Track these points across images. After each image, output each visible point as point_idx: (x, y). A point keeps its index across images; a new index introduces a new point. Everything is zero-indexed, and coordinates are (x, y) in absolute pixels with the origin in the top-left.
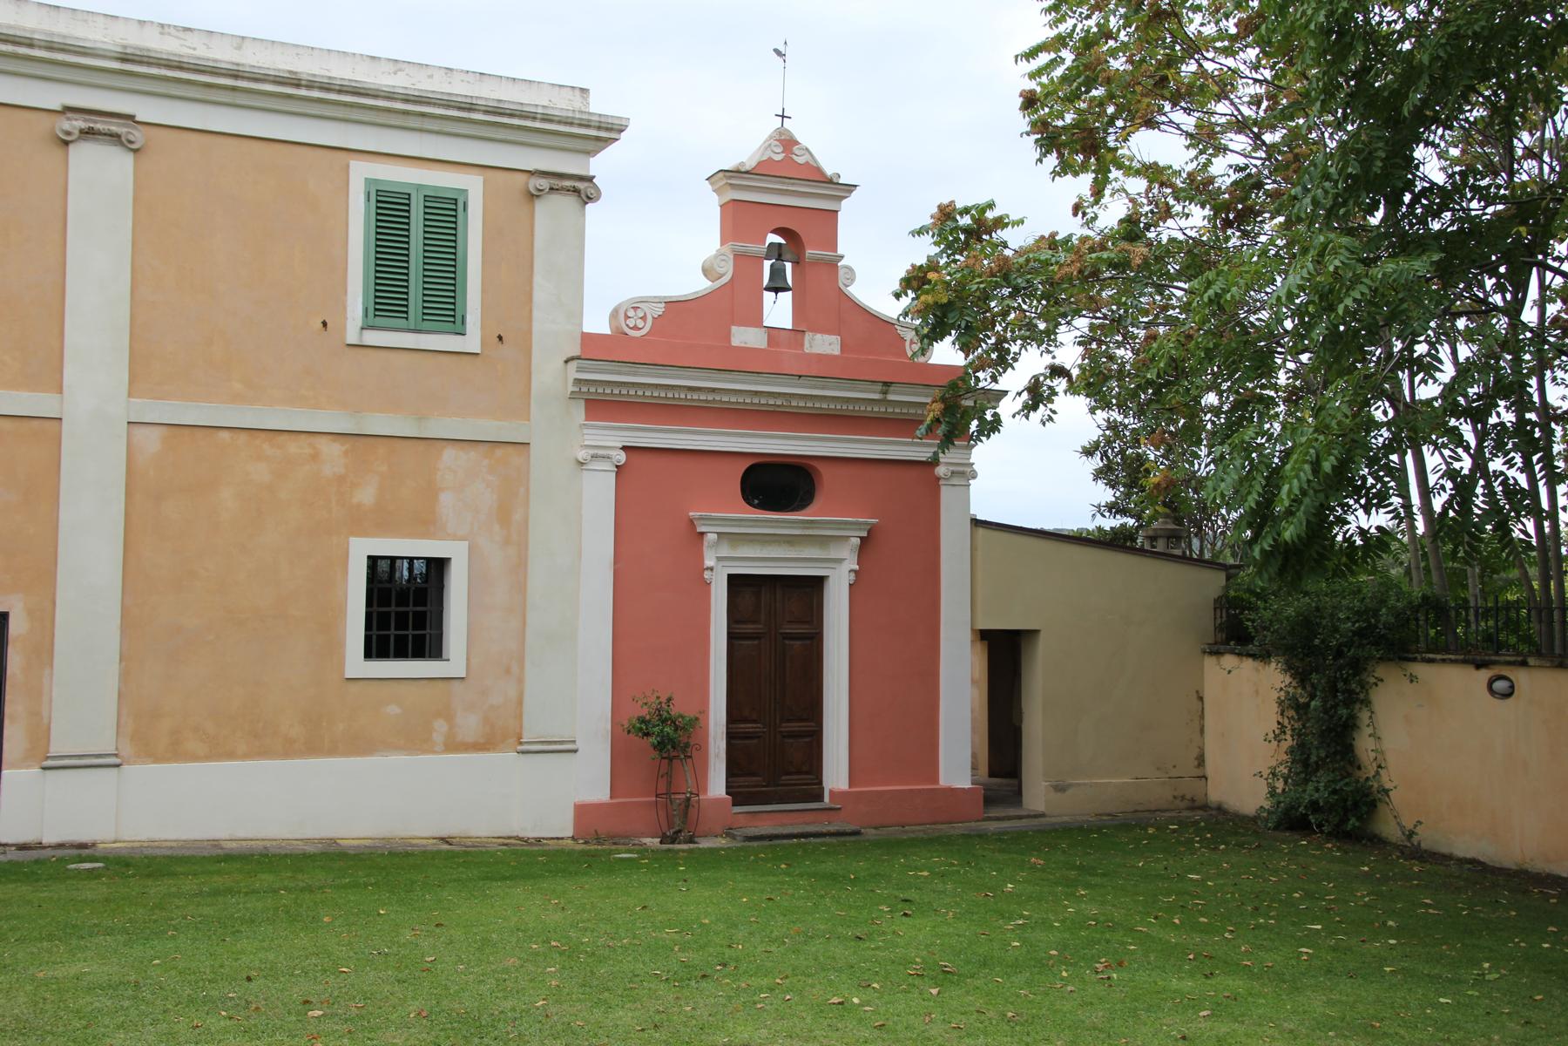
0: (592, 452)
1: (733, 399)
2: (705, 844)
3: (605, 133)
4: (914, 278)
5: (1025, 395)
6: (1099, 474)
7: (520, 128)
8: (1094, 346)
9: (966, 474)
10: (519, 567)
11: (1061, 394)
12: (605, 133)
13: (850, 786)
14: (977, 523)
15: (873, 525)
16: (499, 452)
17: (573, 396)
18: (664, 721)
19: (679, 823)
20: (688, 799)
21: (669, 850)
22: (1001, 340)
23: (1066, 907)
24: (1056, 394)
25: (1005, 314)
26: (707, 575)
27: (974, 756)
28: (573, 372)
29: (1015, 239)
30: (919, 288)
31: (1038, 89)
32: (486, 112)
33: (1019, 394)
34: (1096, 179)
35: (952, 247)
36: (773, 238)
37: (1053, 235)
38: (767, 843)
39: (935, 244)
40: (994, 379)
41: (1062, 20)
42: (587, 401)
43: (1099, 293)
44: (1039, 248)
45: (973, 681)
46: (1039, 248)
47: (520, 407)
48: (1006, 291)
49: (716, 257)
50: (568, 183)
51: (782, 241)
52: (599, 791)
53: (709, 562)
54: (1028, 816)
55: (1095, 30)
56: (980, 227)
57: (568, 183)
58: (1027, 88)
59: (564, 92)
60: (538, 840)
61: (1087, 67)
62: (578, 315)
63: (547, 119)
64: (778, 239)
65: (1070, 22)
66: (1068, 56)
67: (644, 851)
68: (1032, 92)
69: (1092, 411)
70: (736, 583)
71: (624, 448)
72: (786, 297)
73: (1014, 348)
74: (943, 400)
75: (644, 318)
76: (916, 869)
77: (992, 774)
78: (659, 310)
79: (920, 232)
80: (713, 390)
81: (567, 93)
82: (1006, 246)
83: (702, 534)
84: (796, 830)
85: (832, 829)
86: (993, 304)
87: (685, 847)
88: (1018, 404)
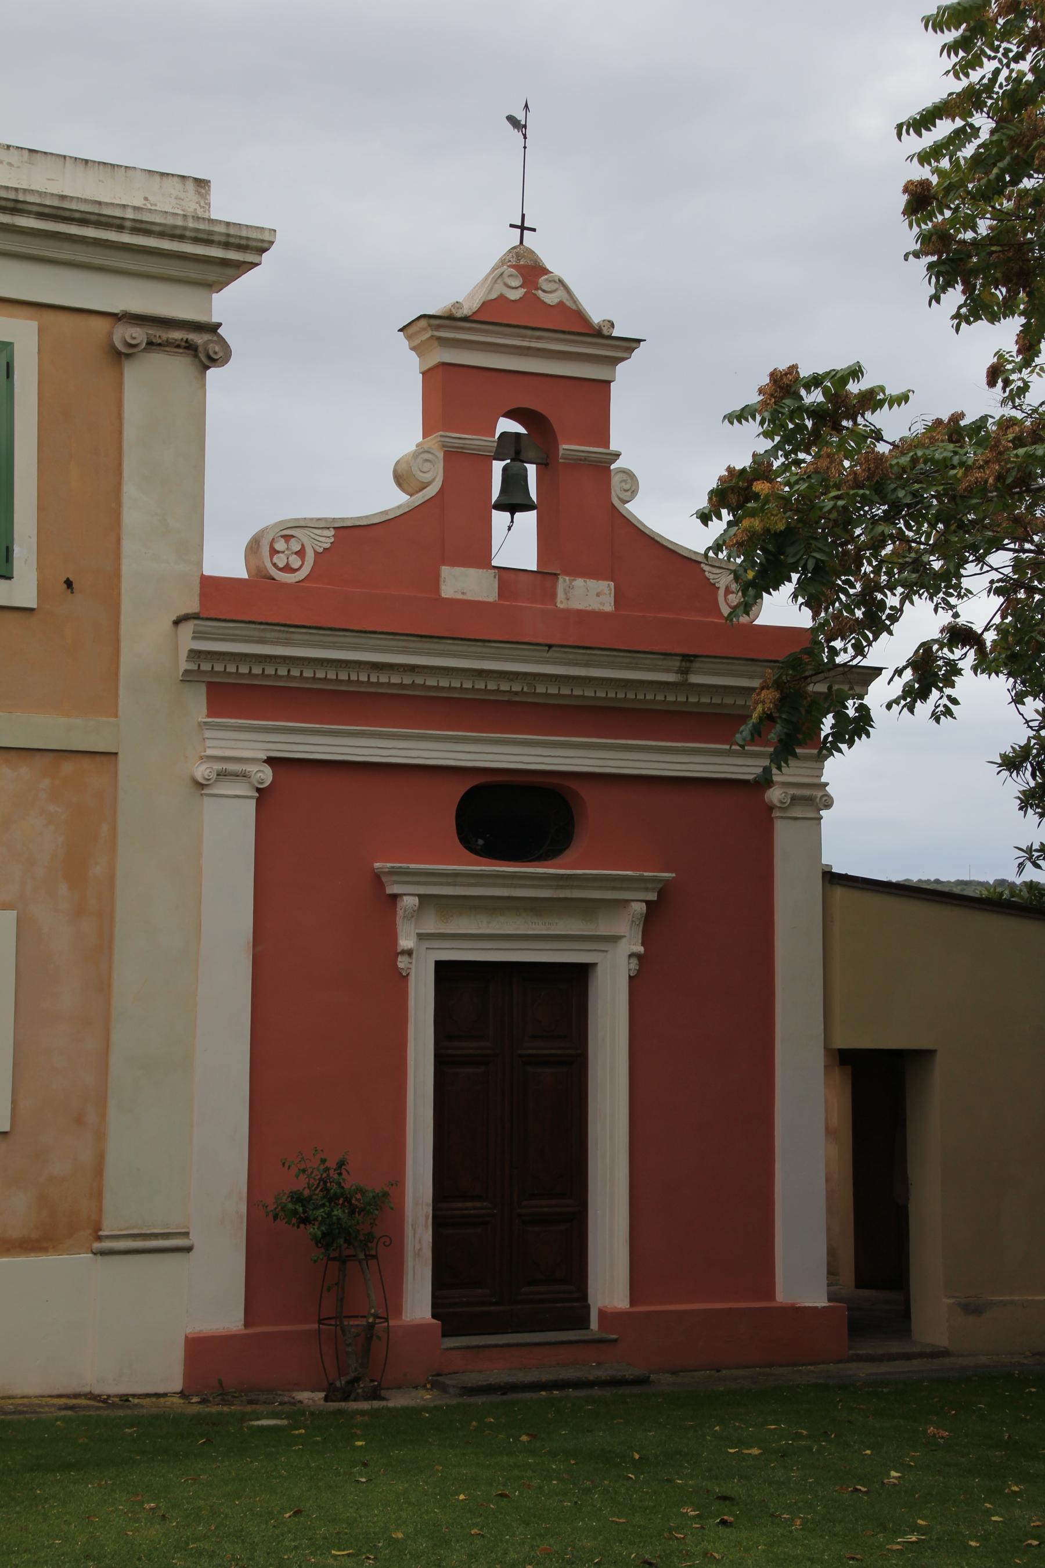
0: (218, 766)
1: (444, 683)
2: (398, 1401)
3: (238, 252)
4: (733, 489)
5: (908, 675)
6: (1028, 800)
7: (97, 242)
8: (1021, 595)
9: (816, 799)
10: (99, 954)
11: (968, 672)
12: (238, 252)
13: (632, 1303)
14: (832, 879)
15: (667, 882)
16: (68, 767)
17: (188, 678)
18: (332, 1199)
19: (356, 1361)
20: (371, 1327)
21: (339, 1412)
22: (871, 587)
23: (989, 1513)
24: (958, 672)
25: (876, 545)
26: (402, 962)
27: (832, 1253)
28: (187, 639)
29: (894, 426)
30: (740, 506)
31: (935, 180)
32: (41, 216)
33: (899, 672)
34: (1026, 327)
35: (792, 441)
36: (507, 425)
37: (956, 418)
38: (496, 1398)
39: (767, 435)
40: (859, 650)
41: (975, 62)
42: (209, 685)
43: (1030, 508)
44: (933, 441)
45: (829, 1132)
46: (933, 441)
47: (102, 695)
48: (879, 510)
49: (416, 455)
50: (177, 335)
51: (521, 430)
52: (227, 1317)
53: (406, 942)
54: (921, 1355)
55: (1030, 77)
56: (836, 408)
57: (177, 335)
58: (916, 178)
59: (168, 182)
60: (125, 1398)
61: (1014, 141)
62: (194, 546)
63: (141, 228)
64: (514, 427)
65: (989, 66)
66: (984, 123)
67: (297, 1414)
68: (925, 184)
69: (1018, 699)
70: (447, 973)
71: (270, 761)
72: (528, 520)
73: (892, 601)
74: (778, 685)
75: (301, 553)
76: (740, 1443)
77: (860, 1284)
78: (326, 539)
79: (741, 416)
80: (412, 669)
81: (173, 187)
82: (878, 436)
83: (395, 897)
84: (546, 1376)
85: (603, 1374)
86: (858, 531)
87: (365, 1405)
88: (897, 687)
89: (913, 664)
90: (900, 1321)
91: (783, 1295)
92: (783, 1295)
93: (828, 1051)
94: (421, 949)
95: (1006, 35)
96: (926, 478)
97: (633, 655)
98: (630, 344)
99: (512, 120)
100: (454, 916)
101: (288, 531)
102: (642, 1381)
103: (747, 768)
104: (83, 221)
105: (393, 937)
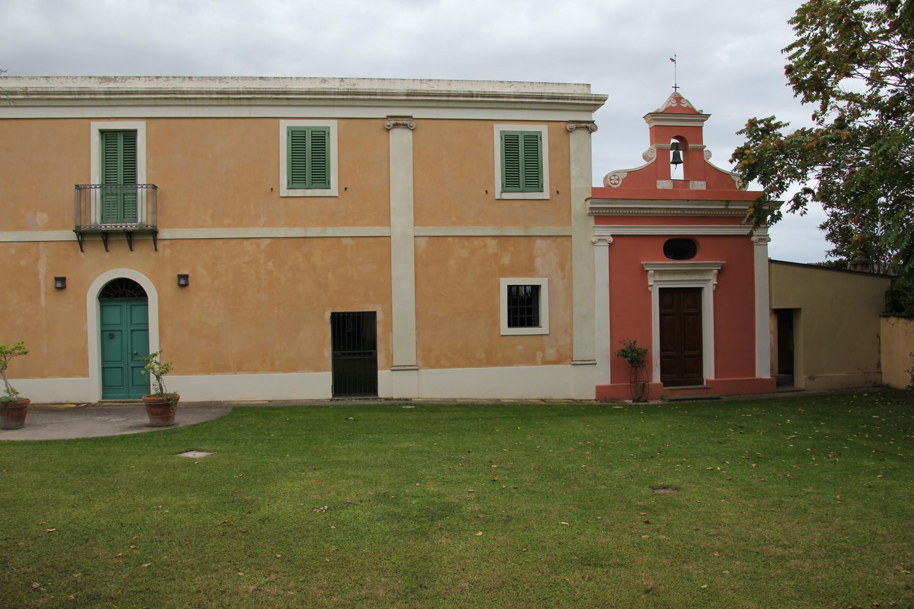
2: (652, 403)
3: (598, 102)
5: (792, 203)
9: (766, 239)
10: (569, 288)
12: (598, 102)
14: (771, 261)
16: (559, 240)
17: (589, 215)
18: (633, 351)
19: (641, 393)
22: (780, 178)
25: (781, 167)
26: (650, 288)
27: (772, 365)
35: (755, 138)
36: (674, 141)
37: (804, 129)
40: (778, 196)
41: (803, 32)
45: (771, 332)
47: (567, 219)
48: (782, 156)
51: (677, 141)
52: (606, 381)
53: (650, 283)
57: (583, 125)
60: (581, 400)
62: (589, 180)
65: (807, 33)
66: (807, 48)
67: (625, 405)
68: (791, 66)
69: (825, 208)
71: (612, 236)
72: (681, 166)
73: (787, 182)
74: (754, 207)
75: (618, 179)
76: (745, 413)
77: (780, 372)
78: (625, 175)
79: (740, 133)
80: (650, 209)
82: (781, 135)
89: (794, 200)
90: (791, 382)
91: (758, 376)
92: (758, 376)
93: (771, 309)
94: (655, 285)
95: (811, 24)
96: (795, 146)
97: (712, 201)
98: (708, 116)
99: (672, 60)
100: (662, 276)
101: (615, 174)
102: (718, 398)
103: (745, 231)
104: (558, 99)
105: (647, 282)
